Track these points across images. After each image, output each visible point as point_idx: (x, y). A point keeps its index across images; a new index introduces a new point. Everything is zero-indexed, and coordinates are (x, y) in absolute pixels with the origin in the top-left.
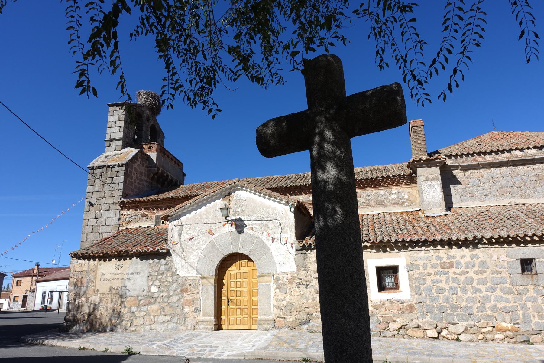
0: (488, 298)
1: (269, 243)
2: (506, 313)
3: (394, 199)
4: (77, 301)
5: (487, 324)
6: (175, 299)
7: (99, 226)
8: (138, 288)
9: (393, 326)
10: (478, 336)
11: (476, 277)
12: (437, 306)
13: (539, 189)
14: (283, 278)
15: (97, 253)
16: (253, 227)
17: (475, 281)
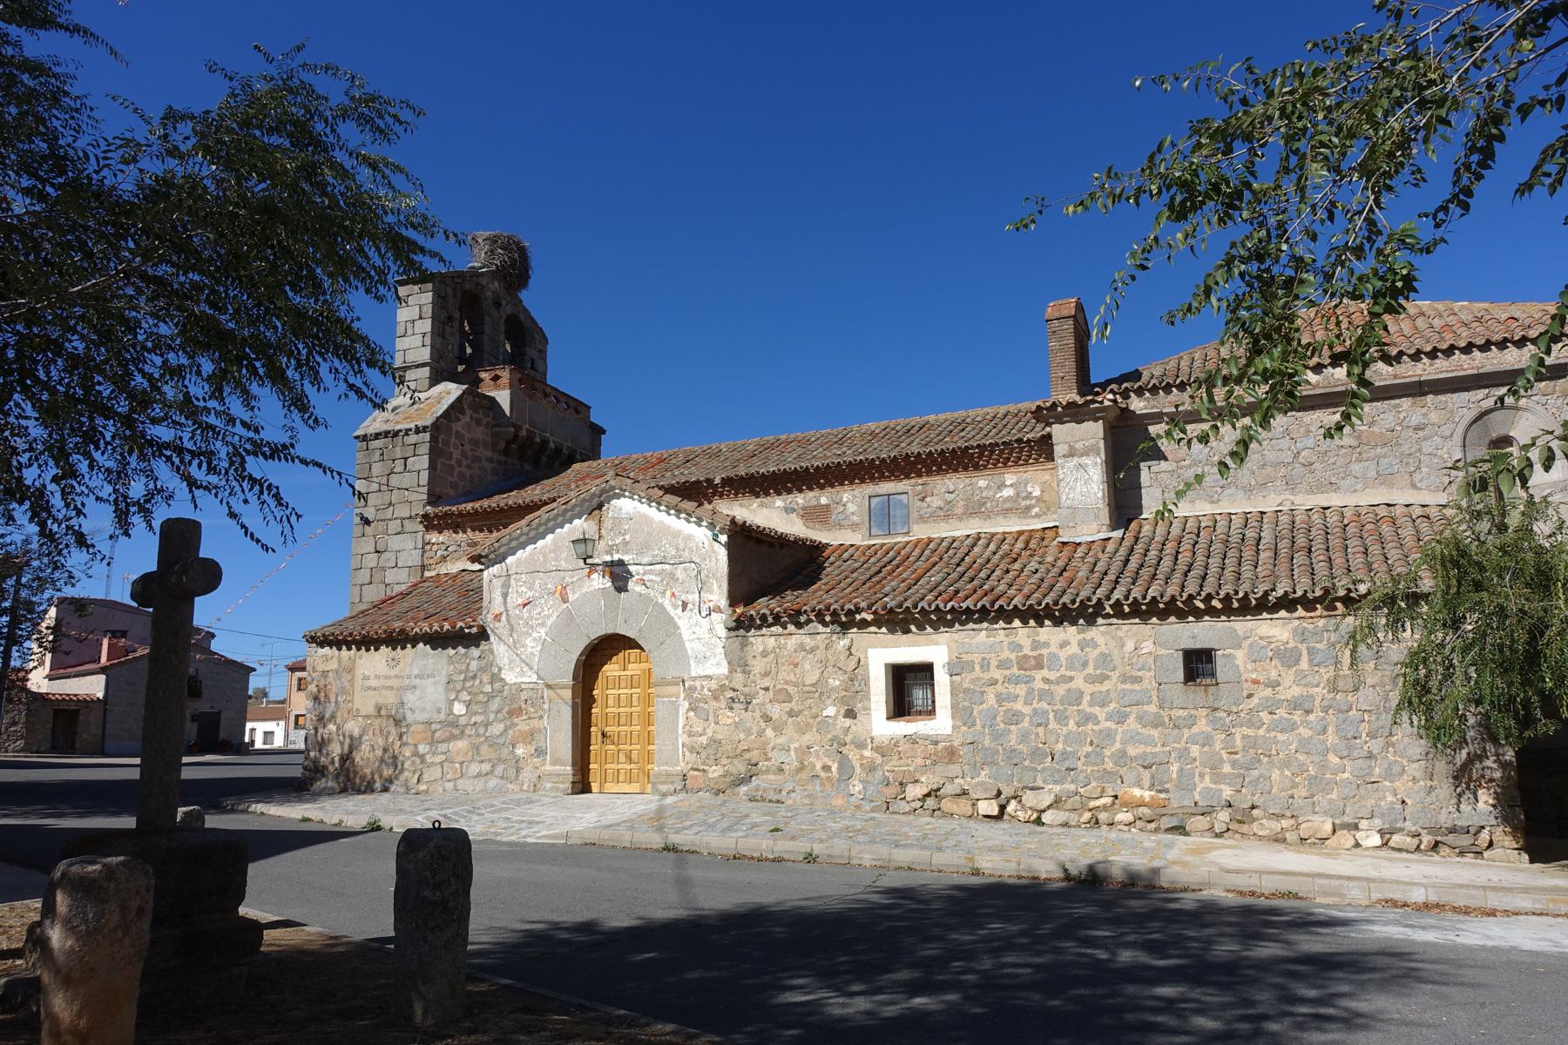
0: (1109, 735)
1: (676, 613)
2: (1145, 767)
3: (1009, 499)
4: (320, 731)
5: (1103, 790)
6: (497, 729)
7: (384, 569)
8: (429, 706)
9: (914, 791)
10: (1080, 816)
11: (1088, 689)
12: (1004, 750)
13: (1356, 468)
14: (703, 687)
15: (351, 634)
16: (645, 578)
17: (1087, 698)
